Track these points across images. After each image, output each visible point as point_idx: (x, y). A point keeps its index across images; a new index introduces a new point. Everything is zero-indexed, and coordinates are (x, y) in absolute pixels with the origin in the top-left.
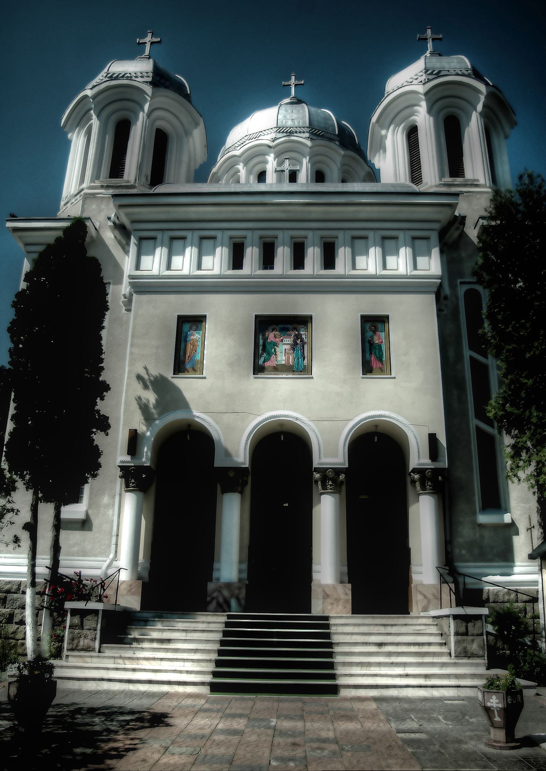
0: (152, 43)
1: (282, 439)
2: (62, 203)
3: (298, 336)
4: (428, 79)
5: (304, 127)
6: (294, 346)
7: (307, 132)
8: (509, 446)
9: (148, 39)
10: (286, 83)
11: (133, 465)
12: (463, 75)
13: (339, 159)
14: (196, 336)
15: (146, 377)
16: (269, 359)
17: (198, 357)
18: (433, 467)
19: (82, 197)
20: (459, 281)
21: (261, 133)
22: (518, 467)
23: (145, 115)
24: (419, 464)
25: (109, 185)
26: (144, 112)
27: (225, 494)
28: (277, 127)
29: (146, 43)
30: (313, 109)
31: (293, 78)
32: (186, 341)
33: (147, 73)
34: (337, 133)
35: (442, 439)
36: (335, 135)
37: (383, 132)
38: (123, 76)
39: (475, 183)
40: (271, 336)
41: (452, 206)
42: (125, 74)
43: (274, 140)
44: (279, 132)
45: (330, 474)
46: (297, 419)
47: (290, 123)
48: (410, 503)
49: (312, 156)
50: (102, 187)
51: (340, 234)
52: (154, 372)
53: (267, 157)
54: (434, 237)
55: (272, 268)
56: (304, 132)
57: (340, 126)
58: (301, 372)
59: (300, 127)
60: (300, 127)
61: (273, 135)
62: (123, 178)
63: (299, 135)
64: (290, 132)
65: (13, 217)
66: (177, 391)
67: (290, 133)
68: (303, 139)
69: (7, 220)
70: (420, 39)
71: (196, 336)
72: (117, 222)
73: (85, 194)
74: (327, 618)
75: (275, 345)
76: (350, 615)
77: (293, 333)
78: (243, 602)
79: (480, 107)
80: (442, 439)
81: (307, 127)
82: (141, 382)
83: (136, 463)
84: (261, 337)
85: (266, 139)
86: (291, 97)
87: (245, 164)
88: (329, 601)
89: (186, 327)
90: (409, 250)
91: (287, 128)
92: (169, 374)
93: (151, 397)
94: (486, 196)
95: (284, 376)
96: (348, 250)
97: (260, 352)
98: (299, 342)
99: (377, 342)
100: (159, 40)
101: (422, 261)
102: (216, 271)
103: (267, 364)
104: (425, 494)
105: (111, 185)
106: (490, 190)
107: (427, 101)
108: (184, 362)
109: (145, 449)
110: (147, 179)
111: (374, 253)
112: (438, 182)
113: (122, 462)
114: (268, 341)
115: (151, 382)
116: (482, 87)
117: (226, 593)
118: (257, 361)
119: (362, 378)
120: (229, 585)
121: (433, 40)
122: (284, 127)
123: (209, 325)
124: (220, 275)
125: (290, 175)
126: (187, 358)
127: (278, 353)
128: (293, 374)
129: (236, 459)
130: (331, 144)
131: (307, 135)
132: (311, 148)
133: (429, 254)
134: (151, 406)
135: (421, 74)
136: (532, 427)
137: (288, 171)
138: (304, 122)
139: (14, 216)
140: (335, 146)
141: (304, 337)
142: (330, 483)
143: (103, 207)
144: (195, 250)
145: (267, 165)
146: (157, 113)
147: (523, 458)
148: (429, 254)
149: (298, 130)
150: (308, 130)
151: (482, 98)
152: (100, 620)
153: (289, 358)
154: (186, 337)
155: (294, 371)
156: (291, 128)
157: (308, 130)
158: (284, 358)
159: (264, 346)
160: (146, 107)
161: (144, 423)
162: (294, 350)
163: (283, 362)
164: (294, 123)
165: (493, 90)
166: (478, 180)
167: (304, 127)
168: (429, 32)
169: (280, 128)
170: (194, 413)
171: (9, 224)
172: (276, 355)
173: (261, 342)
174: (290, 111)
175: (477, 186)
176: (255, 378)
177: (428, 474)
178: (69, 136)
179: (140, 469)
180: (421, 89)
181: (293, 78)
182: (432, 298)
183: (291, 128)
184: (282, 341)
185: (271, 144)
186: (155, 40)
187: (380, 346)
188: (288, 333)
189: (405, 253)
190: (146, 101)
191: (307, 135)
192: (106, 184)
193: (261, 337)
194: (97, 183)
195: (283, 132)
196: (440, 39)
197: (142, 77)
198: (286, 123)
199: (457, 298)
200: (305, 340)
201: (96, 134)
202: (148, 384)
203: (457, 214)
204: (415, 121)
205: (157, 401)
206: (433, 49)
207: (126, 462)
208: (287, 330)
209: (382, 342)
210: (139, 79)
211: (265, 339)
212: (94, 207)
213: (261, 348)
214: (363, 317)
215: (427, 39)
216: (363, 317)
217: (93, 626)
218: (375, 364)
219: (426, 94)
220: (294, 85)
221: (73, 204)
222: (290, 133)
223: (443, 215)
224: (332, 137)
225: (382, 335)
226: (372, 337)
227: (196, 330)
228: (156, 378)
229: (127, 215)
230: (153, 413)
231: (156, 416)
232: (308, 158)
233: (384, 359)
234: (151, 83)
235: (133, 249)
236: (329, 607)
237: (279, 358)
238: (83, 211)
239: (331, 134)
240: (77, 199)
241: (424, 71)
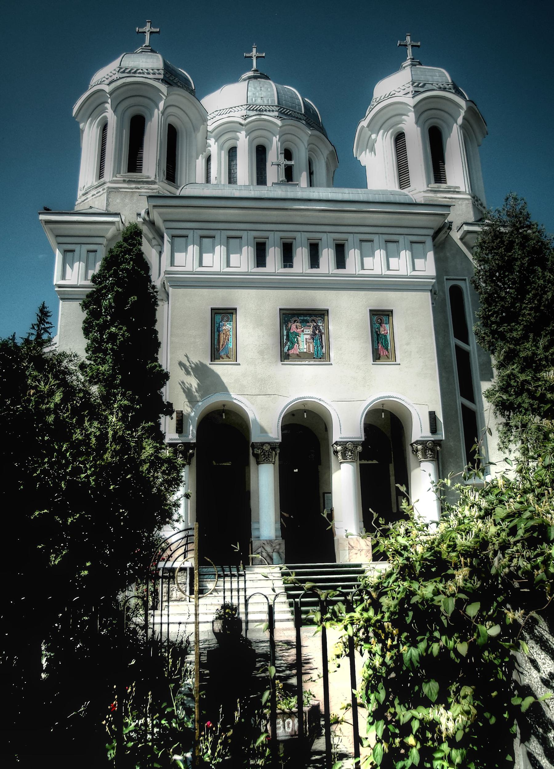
0: (151, 33)
1: (305, 417)
2: (80, 193)
3: (316, 327)
4: (415, 91)
5: (273, 106)
6: (314, 335)
7: (276, 111)
8: (501, 424)
9: (147, 28)
10: (248, 55)
11: (180, 441)
12: (444, 89)
13: (306, 139)
14: (228, 326)
15: (188, 364)
16: (292, 348)
17: (231, 345)
18: (433, 439)
19: (105, 191)
20: (445, 277)
21: (231, 110)
22: (510, 441)
23: (160, 112)
24: (422, 437)
25: (131, 179)
26: (159, 110)
27: (259, 465)
28: (247, 105)
29: (145, 32)
30: (280, 86)
31: (254, 50)
32: (219, 331)
33: (158, 70)
34: (303, 112)
35: (440, 416)
36: (301, 114)
37: (374, 136)
38: (135, 73)
39: (457, 190)
40: (293, 327)
41: (444, 216)
42: (138, 70)
43: (246, 117)
44: (249, 110)
45: (350, 446)
46: (320, 400)
47: (259, 101)
48: (410, 469)
49: (282, 135)
50: (124, 181)
51: (350, 237)
52: (195, 359)
53: (238, 134)
54: (429, 242)
55: (291, 266)
56: (273, 111)
57: (306, 105)
58: (320, 358)
59: (269, 106)
60: (269, 106)
61: (244, 113)
62: (141, 172)
63: (268, 113)
64: (260, 110)
65: (47, 211)
66: (217, 377)
67: (261, 111)
68: (272, 117)
69: (40, 213)
70: (400, 45)
71: (228, 326)
72: (147, 219)
73: (109, 188)
74: (359, 566)
75: (297, 335)
76: (371, 562)
77: (312, 325)
78: (283, 556)
79: (460, 120)
80: (440, 416)
81: (276, 106)
82: (183, 368)
83: (185, 440)
84: (284, 328)
85: (237, 116)
86: (253, 69)
87: (216, 141)
88: (354, 551)
89: (218, 318)
90: (408, 253)
91: (257, 105)
92: (207, 361)
93: (193, 382)
94: (467, 202)
95: (307, 363)
96: (357, 252)
97: (285, 341)
98: (317, 332)
99: (383, 333)
100: (158, 30)
101: (419, 262)
102: (244, 269)
103: (291, 352)
104: (426, 461)
105: (133, 179)
106: (469, 197)
107: (415, 112)
108: (218, 350)
109: (191, 428)
110: (164, 174)
111: (380, 254)
112: (426, 188)
113: (171, 439)
114: (291, 331)
115: (192, 368)
116: (463, 103)
117: (269, 549)
118: (282, 349)
119: (373, 364)
120: (270, 542)
121: (412, 46)
122: (253, 105)
123: (240, 317)
124: (248, 272)
125: (285, 169)
126: (221, 346)
127: (300, 342)
128: (314, 361)
129: (270, 435)
130: (299, 124)
131: (276, 114)
132: (281, 127)
133: (424, 257)
134: (194, 390)
135: (408, 85)
136: (523, 411)
137: (283, 165)
138: (273, 101)
139: (48, 210)
140: (302, 125)
141: (321, 328)
142: (350, 454)
143: (127, 201)
144: (224, 248)
145: (238, 142)
146: (170, 110)
147: (514, 433)
148: (424, 257)
149: (267, 108)
150: (277, 109)
151: (463, 113)
152: (188, 576)
153: (309, 346)
154: (219, 327)
155: (314, 358)
156: (260, 106)
157: (277, 109)
158: (305, 347)
159: (288, 335)
160: (161, 105)
161: (188, 404)
162: (313, 339)
163: (305, 350)
164: (264, 101)
165: (471, 104)
166: (458, 187)
167: (273, 106)
168: (408, 38)
169: (250, 105)
170: (233, 396)
171: (42, 217)
172: (298, 343)
173: (285, 333)
174: (258, 89)
175: (458, 192)
176: (282, 364)
177: (429, 445)
178: (81, 125)
179: (187, 445)
180: (411, 101)
181: (254, 50)
182: (427, 296)
183: (260, 106)
184: (303, 331)
185: (243, 122)
186: (154, 30)
187: (385, 336)
188: (308, 324)
189: (405, 255)
190: (161, 99)
191: (276, 114)
192: (128, 179)
193: (284, 328)
194: (119, 178)
195: (253, 110)
196: (418, 46)
197: (154, 74)
198: (255, 101)
199: (444, 292)
200: (323, 331)
201: (115, 129)
202: (190, 370)
203: (446, 221)
204: (402, 128)
205: (198, 385)
206: (412, 55)
207: (175, 439)
208: (307, 321)
209: (387, 333)
210: (151, 76)
211: (288, 330)
212: (118, 201)
213: (285, 337)
214: (371, 311)
215: (406, 45)
216: (371, 311)
217: (183, 581)
218: (383, 352)
219: (414, 107)
220: (255, 57)
221: (94, 196)
222: (261, 111)
223: (436, 223)
224: (299, 116)
225: (387, 326)
226: (379, 328)
227: (227, 321)
228: (196, 365)
229: (160, 214)
230: (195, 396)
231: (198, 399)
232: (278, 136)
233: (389, 348)
234: (163, 80)
235: (167, 247)
236: (354, 556)
237: (301, 347)
238: (108, 205)
239: (298, 113)
240: (100, 192)
241: (411, 83)
